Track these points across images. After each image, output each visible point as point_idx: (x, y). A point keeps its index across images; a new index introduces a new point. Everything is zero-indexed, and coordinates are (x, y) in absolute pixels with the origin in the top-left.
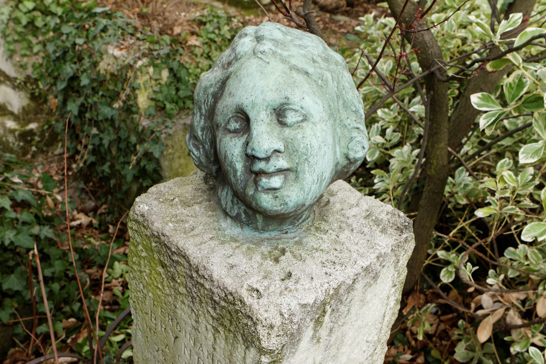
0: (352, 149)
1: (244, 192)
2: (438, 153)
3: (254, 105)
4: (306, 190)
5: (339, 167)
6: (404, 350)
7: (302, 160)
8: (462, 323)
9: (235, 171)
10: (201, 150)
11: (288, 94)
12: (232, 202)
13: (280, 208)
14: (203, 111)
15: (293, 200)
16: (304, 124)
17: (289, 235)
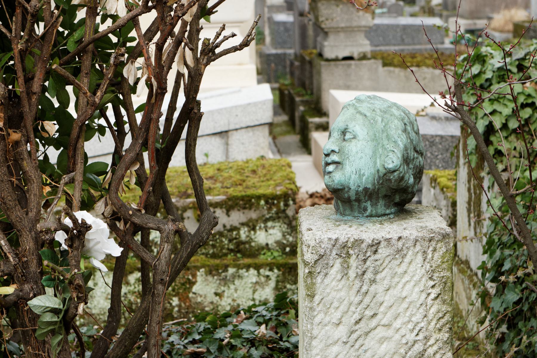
4: (347, 176)
5: (381, 175)
16: (353, 140)
17: (359, 220)
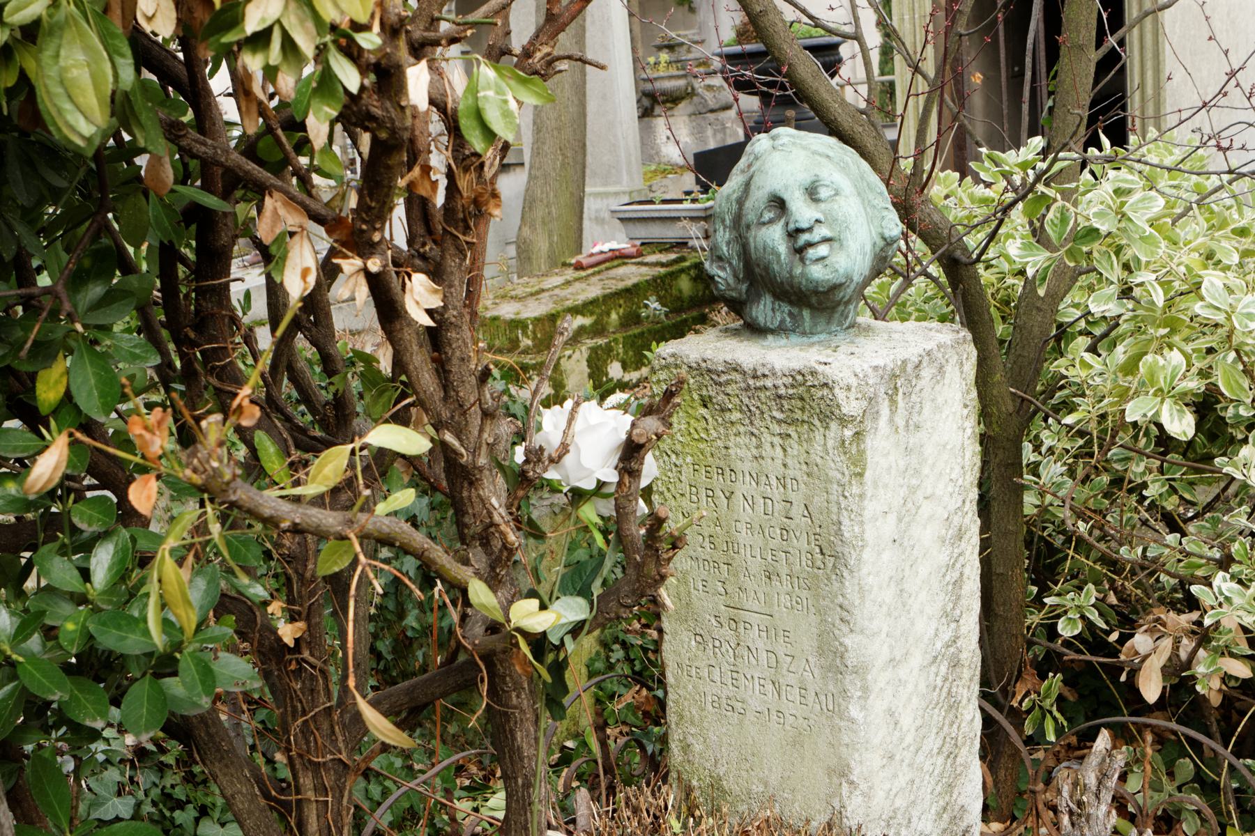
1: (791, 276)
2: (995, 392)
5: (878, 249)
9: (778, 255)
11: (817, 171)
12: (773, 310)
14: (728, 222)
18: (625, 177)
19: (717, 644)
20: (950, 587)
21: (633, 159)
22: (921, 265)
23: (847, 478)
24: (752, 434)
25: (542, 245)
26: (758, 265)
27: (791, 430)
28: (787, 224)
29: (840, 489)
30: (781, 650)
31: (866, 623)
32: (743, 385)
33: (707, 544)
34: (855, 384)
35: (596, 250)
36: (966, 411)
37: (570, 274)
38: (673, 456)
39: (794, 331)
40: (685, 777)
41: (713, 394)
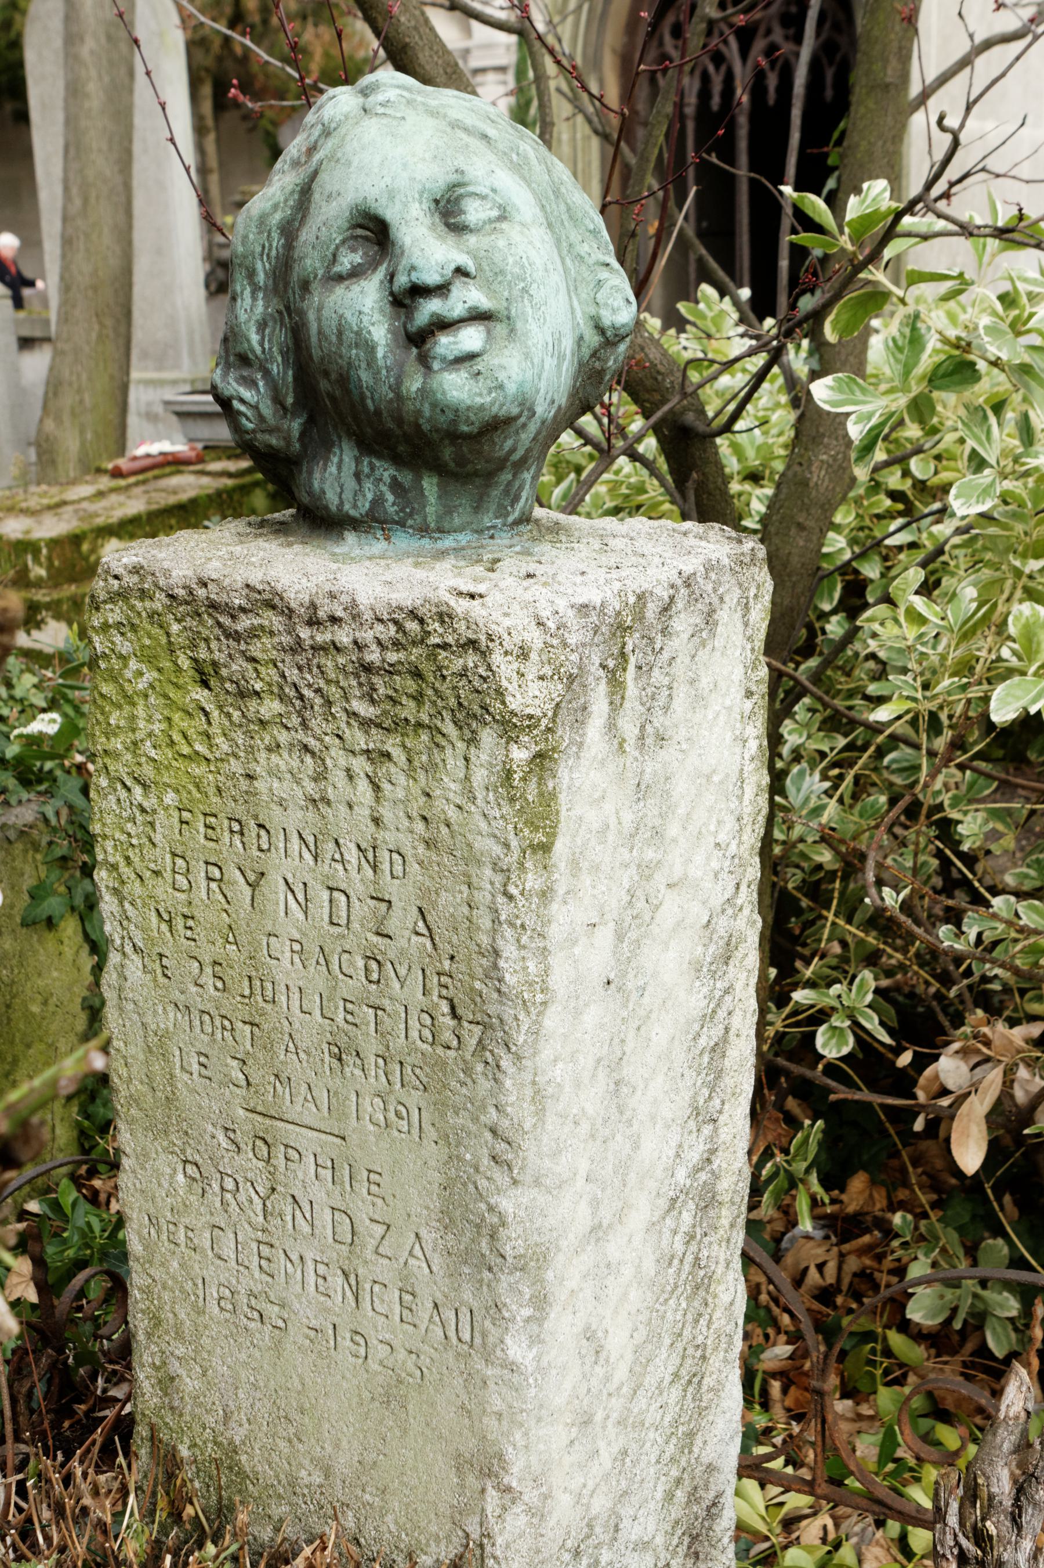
0: (606, 304)
1: (399, 397)
3: (391, 194)
5: (586, 352)
6: (767, 1337)
7: (516, 292)
8: (904, 1218)
10: (261, 384)
11: (461, 162)
12: (357, 476)
13: (488, 399)
14: (261, 278)
15: (514, 376)
16: (504, 225)
18: (186, 361)
19: (229, 1184)
20: (706, 1058)
21: (197, 337)
22: (624, 437)
23: (516, 854)
24: (306, 748)
25: (70, 444)
26: (326, 374)
27: (392, 745)
28: (391, 277)
29: (498, 879)
30: (362, 1210)
31: (547, 1163)
32: (286, 640)
33: (207, 979)
34: (538, 644)
35: (140, 451)
36: (748, 705)
37: (105, 482)
38: (138, 790)
39: (402, 524)
40: (165, 1437)
41: (220, 657)
